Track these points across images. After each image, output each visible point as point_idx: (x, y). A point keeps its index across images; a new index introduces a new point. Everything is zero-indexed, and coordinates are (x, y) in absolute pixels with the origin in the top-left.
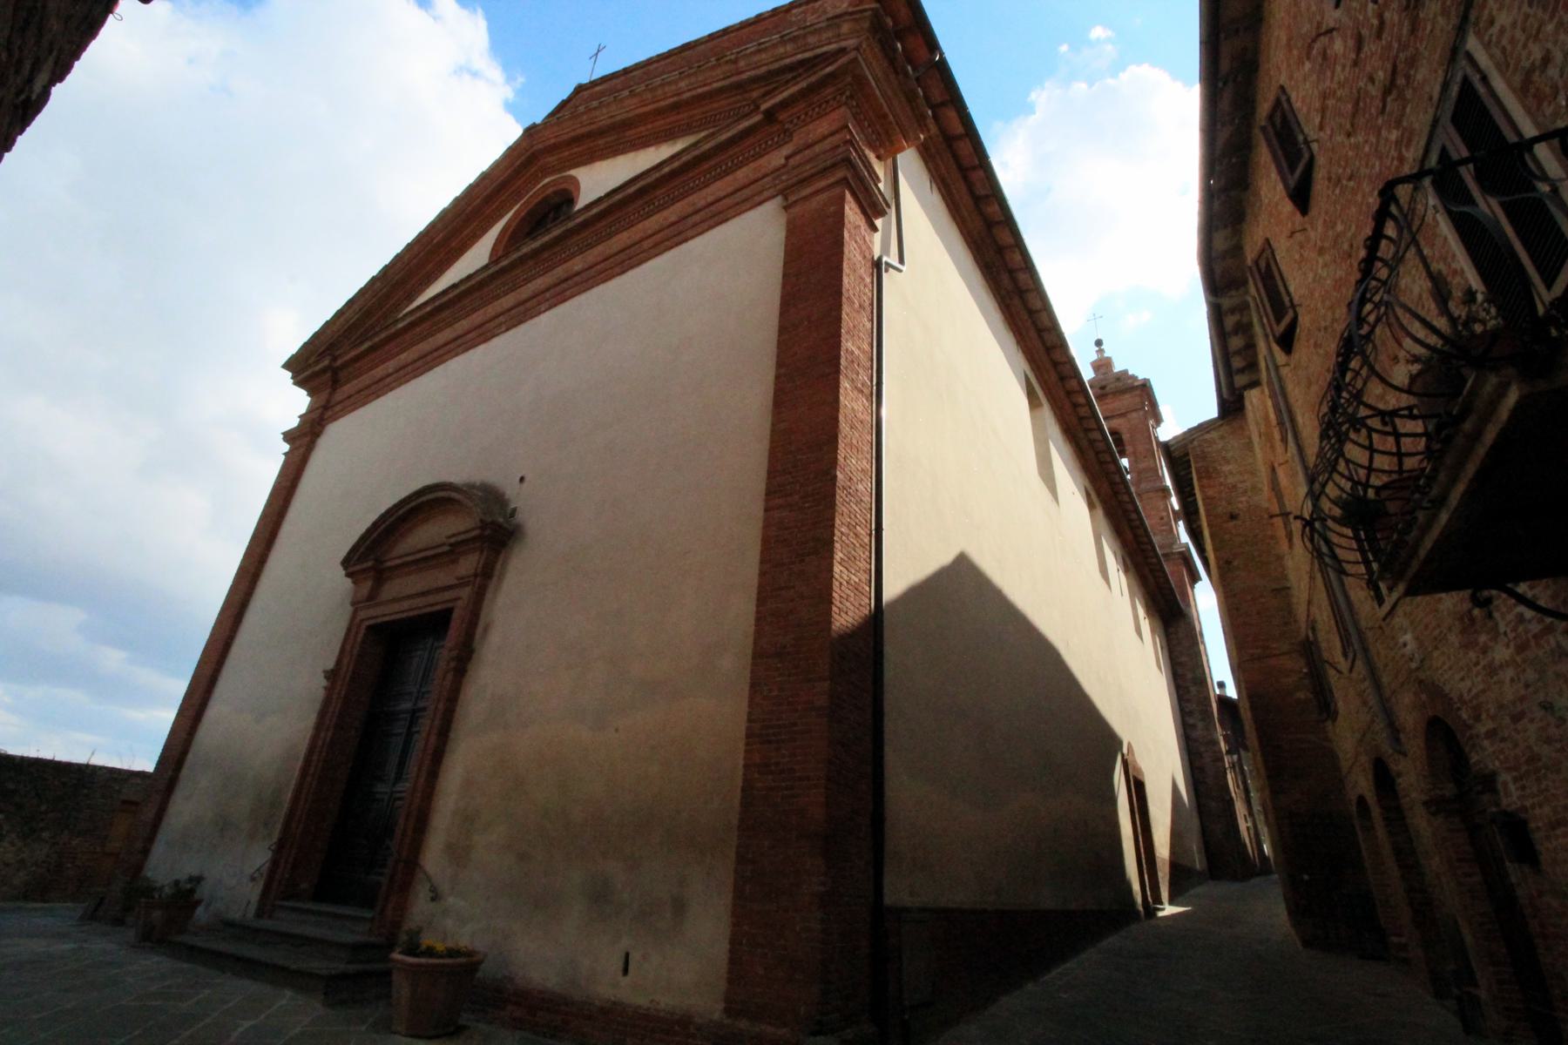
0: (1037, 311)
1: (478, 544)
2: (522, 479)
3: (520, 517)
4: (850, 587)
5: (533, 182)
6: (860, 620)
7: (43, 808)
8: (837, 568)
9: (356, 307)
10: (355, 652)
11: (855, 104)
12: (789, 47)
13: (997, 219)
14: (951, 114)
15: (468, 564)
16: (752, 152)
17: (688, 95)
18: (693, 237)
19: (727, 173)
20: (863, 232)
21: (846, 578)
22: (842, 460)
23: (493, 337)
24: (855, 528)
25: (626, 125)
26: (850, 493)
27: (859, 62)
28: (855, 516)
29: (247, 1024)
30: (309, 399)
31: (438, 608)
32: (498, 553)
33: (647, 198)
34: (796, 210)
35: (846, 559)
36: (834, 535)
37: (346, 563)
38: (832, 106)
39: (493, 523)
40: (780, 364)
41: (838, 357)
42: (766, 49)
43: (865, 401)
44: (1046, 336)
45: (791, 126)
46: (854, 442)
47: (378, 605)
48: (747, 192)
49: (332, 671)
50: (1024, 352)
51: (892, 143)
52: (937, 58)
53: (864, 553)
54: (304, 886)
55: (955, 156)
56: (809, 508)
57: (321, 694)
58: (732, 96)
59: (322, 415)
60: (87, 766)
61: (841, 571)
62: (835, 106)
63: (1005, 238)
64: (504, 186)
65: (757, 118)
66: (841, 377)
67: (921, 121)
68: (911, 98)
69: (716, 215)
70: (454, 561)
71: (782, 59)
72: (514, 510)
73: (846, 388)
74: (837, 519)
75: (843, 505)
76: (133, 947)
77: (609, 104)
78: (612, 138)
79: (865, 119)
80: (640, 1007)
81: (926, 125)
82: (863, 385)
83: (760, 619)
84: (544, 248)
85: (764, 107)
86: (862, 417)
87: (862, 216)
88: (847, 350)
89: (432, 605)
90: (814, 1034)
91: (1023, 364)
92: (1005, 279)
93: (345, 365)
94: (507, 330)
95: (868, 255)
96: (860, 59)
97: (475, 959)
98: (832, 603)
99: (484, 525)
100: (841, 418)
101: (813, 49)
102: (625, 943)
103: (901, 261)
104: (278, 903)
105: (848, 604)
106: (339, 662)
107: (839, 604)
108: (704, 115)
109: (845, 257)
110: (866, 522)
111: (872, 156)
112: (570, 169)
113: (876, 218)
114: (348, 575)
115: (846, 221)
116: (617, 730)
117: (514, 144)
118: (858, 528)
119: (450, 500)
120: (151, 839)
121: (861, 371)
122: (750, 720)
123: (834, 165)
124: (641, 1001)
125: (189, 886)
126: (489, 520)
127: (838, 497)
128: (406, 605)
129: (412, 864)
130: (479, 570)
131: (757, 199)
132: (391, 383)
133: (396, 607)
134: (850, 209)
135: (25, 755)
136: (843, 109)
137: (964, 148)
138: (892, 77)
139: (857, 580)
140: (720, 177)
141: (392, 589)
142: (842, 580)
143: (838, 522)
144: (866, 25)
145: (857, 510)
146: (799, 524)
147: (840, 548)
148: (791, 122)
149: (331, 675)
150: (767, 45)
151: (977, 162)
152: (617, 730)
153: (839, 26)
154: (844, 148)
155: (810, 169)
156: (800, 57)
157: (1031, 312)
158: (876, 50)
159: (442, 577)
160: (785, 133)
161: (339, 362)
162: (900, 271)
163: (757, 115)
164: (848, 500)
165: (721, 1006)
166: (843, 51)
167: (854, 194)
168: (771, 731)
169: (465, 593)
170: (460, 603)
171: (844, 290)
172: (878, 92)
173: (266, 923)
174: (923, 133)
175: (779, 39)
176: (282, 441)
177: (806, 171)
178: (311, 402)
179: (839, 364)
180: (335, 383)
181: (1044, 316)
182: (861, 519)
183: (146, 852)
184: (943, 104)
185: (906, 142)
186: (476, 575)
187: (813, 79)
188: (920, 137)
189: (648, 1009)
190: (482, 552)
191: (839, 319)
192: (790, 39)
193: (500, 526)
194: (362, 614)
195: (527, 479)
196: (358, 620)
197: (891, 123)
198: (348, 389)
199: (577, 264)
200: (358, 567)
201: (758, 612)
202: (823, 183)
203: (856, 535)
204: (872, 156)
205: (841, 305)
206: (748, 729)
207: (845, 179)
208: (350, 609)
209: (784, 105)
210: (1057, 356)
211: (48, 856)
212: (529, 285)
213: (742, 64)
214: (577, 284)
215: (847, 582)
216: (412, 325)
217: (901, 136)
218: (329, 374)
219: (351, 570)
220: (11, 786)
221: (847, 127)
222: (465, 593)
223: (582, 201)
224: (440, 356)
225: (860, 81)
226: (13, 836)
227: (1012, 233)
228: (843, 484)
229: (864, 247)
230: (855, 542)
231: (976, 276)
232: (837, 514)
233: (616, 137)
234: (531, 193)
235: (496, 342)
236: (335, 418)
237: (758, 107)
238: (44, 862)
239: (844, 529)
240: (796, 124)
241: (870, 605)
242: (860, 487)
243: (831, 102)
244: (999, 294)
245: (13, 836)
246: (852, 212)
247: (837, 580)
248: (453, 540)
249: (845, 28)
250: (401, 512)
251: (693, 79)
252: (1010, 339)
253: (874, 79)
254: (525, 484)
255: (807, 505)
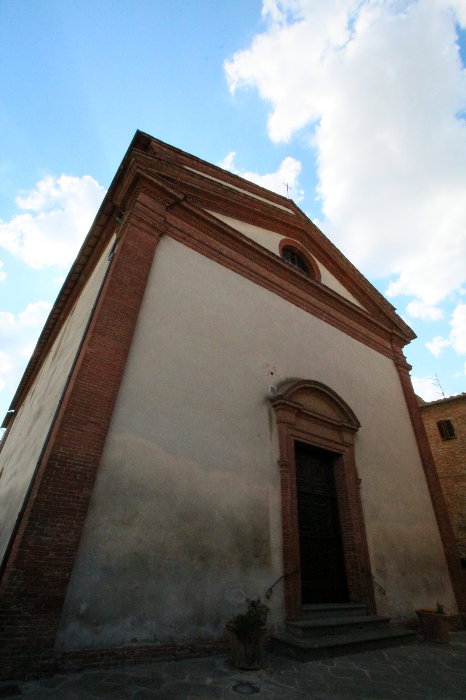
31: (335, 451)
65: (390, 331)
117: (261, 187)
128: (318, 440)
132: (252, 276)
161: (185, 204)
176: (412, 370)
216: (198, 217)
218: (172, 201)
224: (384, 351)
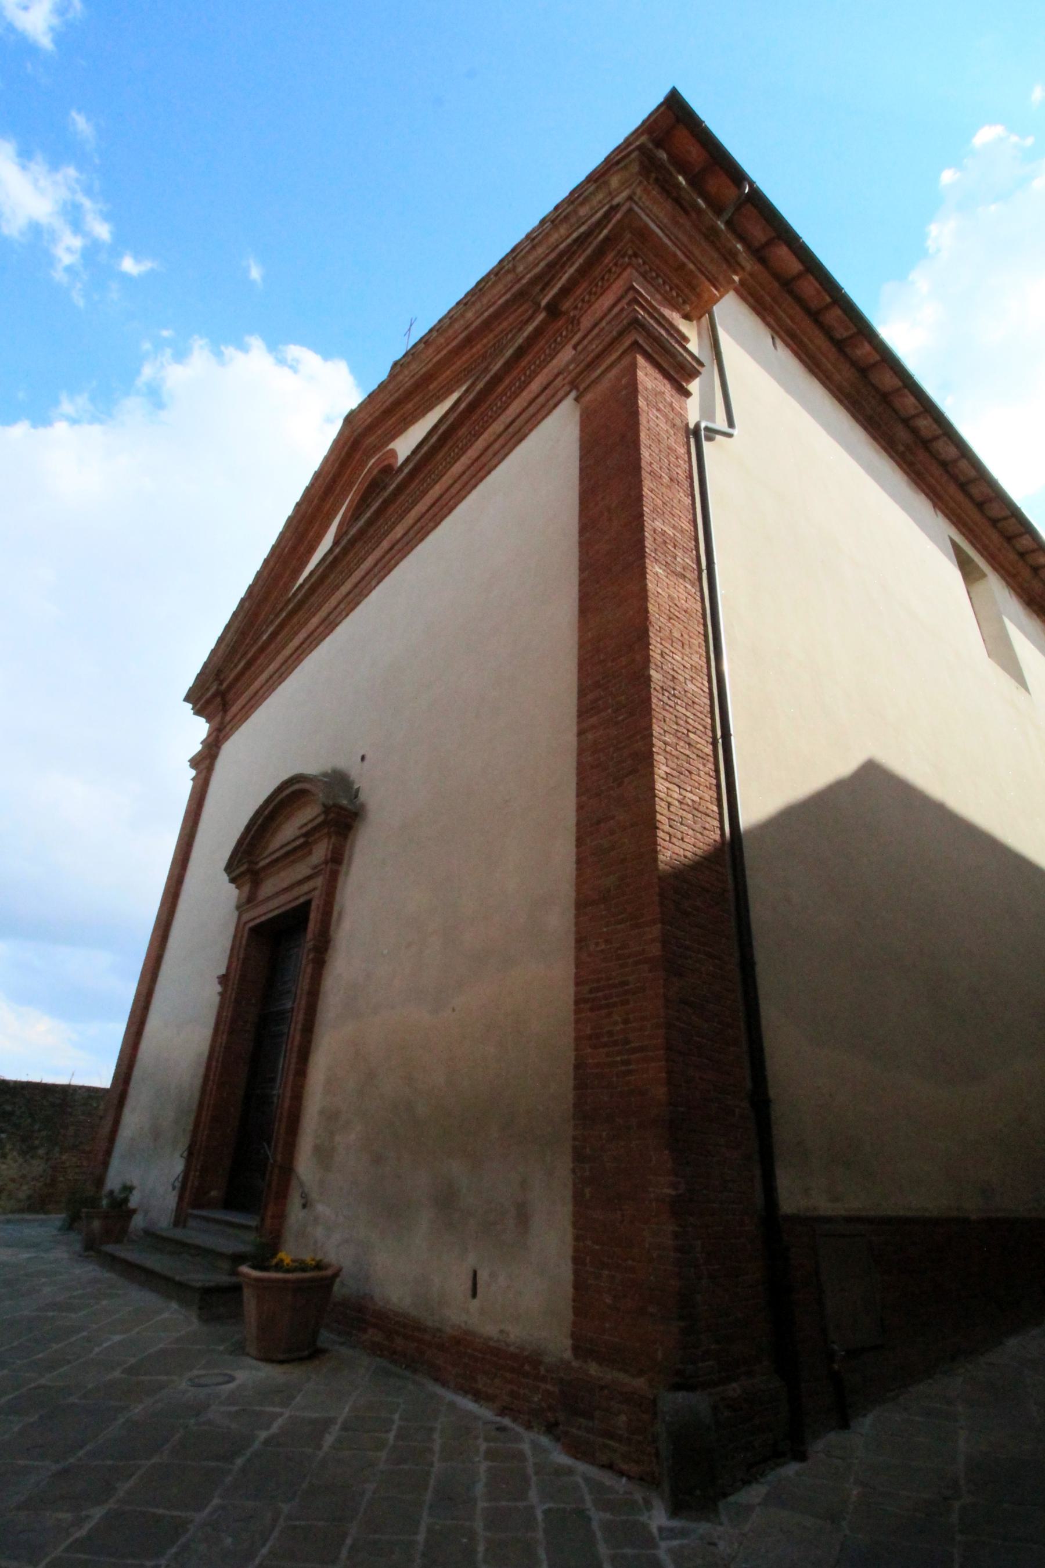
0: (955, 461)
1: (326, 831)
2: (363, 758)
3: (363, 797)
4: (685, 807)
5: (360, 468)
6: (706, 848)
7: (37, 1127)
8: (661, 786)
9: (233, 629)
10: (241, 956)
11: (641, 261)
12: (563, 231)
13: (872, 361)
14: (783, 251)
15: (320, 852)
16: (543, 357)
17: (479, 321)
18: (496, 466)
19: (522, 389)
20: (668, 399)
21: (676, 796)
22: (659, 657)
23: (337, 625)
24: (688, 736)
25: (429, 377)
26: (674, 695)
27: (636, 213)
28: (686, 722)
29: (117, 1338)
30: (207, 725)
32: (346, 837)
33: (450, 443)
34: (589, 397)
35: (675, 773)
36: (653, 745)
37: (229, 868)
38: (615, 272)
39: (335, 805)
40: (582, 569)
41: (641, 541)
42: (540, 242)
43: (689, 587)
44: (975, 491)
45: (576, 312)
46: (677, 634)
47: (257, 906)
48: (542, 399)
49: (223, 975)
50: (946, 516)
51: (699, 296)
52: (747, 191)
53: (704, 765)
54: (214, 1193)
55: (799, 300)
56: (623, 720)
57: (216, 999)
58: (518, 308)
59: (217, 737)
60: (69, 1086)
61: (668, 788)
62: (618, 272)
63: (888, 381)
64: (334, 480)
65: (541, 316)
66: (647, 561)
67: (730, 259)
68: (711, 235)
69: (516, 435)
70: (310, 853)
71: (557, 246)
72: (358, 790)
73: (656, 574)
74: (655, 727)
75: (664, 709)
76: (80, 1256)
77: (409, 363)
78: (418, 398)
79: (658, 276)
80: (490, 1339)
81: (739, 264)
82: (684, 568)
83: (580, 861)
84: (370, 523)
85: (544, 303)
86: (685, 605)
87: (666, 382)
88: (655, 531)
89: (297, 898)
90: (677, 1387)
91: (947, 530)
92: (902, 434)
93: (230, 687)
94: (347, 615)
95: (678, 421)
96: (636, 209)
97: (329, 1272)
98: (658, 828)
99: (327, 809)
100: (652, 608)
101: (587, 221)
102: (471, 1260)
103: (731, 424)
104: (190, 1211)
105: (684, 828)
106: (228, 968)
107: (667, 828)
108: (497, 339)
109: (641, 427)
110: (705, 728)
111: (676, 318)
112: (388, 445)
113: (688, 382)
114: (233, 880)
115: (640, 387)
116: (454, 1010)
118: (691, 735)
119: (303, 792)
120: (109, 1153)
121: (679, 553)
122: (577, 984)
123: (621, 334)
124: (489, 1329)
125: (122, 1196)
126: (331, 803)
127: (654, 700)
129: (287, 1170)
130: (329, 856)
131: (551, 403)
133: (275, 903)
134: (646, 375)
135: (19, 1080)
136: (629, 270)
137: (809, 287)
138: (682, 220)
139: (696, 799)
140: (516, 395)
141: (268, 888)
142: (669, 800)
143: (656, 730)
144: (635, 168)
145: (688, 714)
146: (615, 742)
147: (664, 761)
148: (576, 308)
149: (223, 980)
150: (540, 237)
151: (828, 299)
152: (454, 1010)
153: (606, 183)
154: (630, 309)
155: (597, 347)
156: (575, 235)
157: (944, 465)
158: (654, 193)
159: (302, 870)
160: (572, 323)
161: (225, 685)
162: (730, 435)
163: (539, 314)
164: (672, 704)
165: (569, 1342)
166: (614, 209)
167: (649, 357)
168: (600, 994)
169: (319, 882)
170: (317, 893)
171: (643, 464)
172: (666, 240)
173: (179, 1234)
174: (737, 274)
175: (551, 226)
177: (593, 350)
178: (210, 727)
179: (644, 547)
180: (225, 707)
181: (963, 464)
182: (696, 725)
183: (106, 1164)
184: (769, 243)
185: (717, 289)
186: (326, 862)
187: (589, 252)
188: (734, 280)
189: (498, 1341)
190: (330, 837)
191: (640, 498)
192: (561, 221)
193: (341, 808)
194: (246, 917)
195: (368, 757)
196: (242, 923)
197: (691, 271)
198: (234, 709)
199: (399, 531)
200: (238, 872)
201: (578, 854)
202: (614, 356)
203: (689, 744)
204: (676, 318)
205: (641, 481)
206: (577, 993)
207: (636, 343)
208: (236, 914)
209: (565, 292)
210: (995, 510)
211: (44, 1171)
212: (362, 566)
213: (520, 268)
214: (400, 551)
215: (681, 803)
217: (707, 283)
218: (219, 699)
219: (234, 875)
220: (8, 1108)
221: (633, 288)
222: (319, 882)
223: (401, 458)
225: (643, 235)
226: (15, 1153)
227: (896, 373)
228: (661, 684)
229: (671, 415)
230: (688, 752)
231: (857, 434)
232: (654, 720)
233: (421, 395)
234: (362, 476)
235: (339, 630)
236: (227, 737)
237: (539, 305)
238: (41, 1177)
239: (668, 738)
240: (581, 309)
241: (722, 828)
242: (690, 686)
243: (614, 269)
244: (897, 452)
245: (15, 1153)
246: (648, 378)
247: (661, 799)
248: (304, 830)
249: (614, 182)
250: (266, 812)
251: (478, 305)
252: (922, 504)
253: (658, 226)
254: (366, 762)
255: (620, 718)
